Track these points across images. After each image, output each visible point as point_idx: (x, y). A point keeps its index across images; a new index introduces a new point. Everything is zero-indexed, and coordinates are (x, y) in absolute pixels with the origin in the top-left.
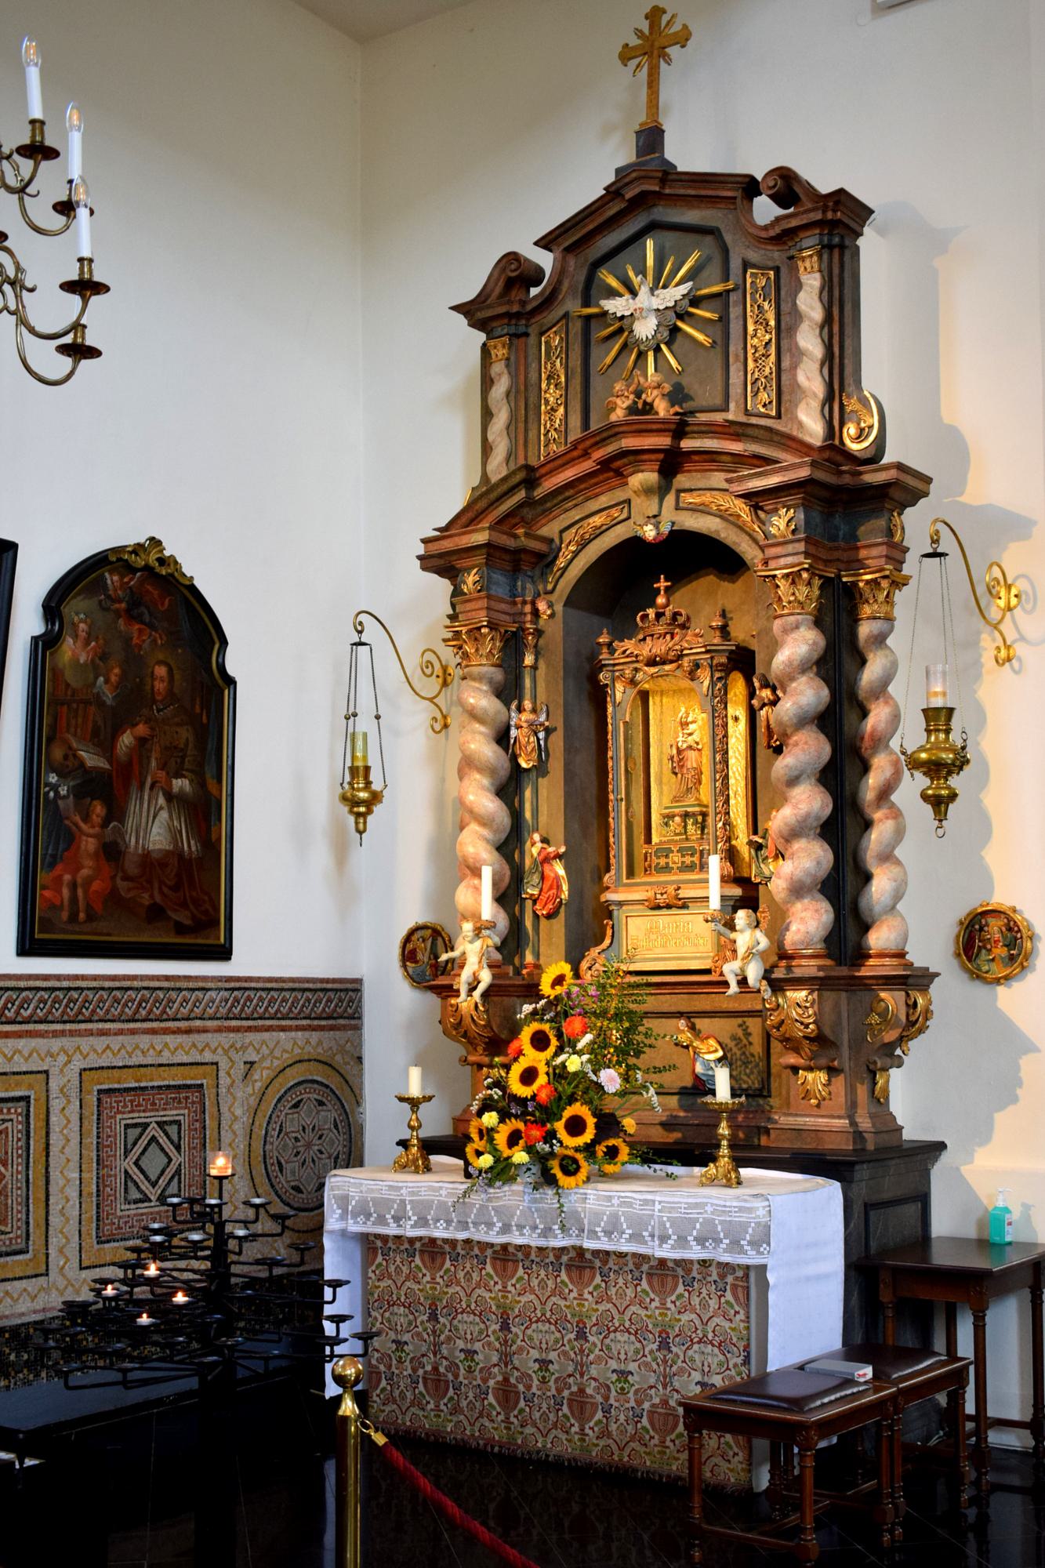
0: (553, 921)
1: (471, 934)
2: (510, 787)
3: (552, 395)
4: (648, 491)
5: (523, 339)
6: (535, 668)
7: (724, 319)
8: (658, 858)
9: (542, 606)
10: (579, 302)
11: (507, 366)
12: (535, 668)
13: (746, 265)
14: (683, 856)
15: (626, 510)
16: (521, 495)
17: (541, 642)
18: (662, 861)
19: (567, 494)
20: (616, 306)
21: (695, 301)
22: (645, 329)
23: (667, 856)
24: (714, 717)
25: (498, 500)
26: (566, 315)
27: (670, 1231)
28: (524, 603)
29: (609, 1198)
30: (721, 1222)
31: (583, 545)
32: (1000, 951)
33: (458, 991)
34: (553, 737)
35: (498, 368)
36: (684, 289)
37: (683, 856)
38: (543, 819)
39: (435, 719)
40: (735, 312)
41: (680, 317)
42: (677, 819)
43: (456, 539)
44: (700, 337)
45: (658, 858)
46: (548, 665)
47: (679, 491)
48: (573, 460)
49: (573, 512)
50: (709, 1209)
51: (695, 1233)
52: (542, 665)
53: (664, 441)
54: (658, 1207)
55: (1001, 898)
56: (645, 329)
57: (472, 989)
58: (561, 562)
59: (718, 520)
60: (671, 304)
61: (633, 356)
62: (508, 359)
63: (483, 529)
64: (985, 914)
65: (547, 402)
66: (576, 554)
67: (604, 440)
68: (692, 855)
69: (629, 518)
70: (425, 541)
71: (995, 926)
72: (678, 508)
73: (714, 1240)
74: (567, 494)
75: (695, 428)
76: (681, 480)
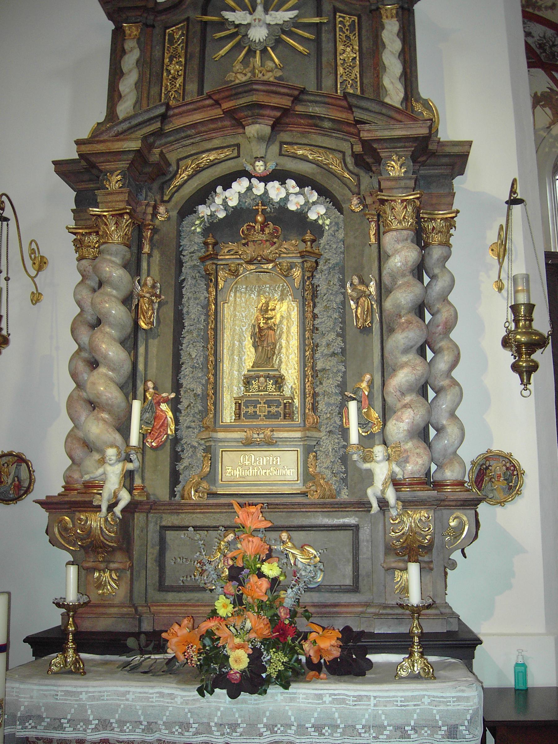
0: (160, 452)
1: (114, 458)
2: (131, 340)
3: (174, 68)
4: (260, 138)
5: (150, 29)
6: (150, 255)
7: (318, 41)
8: (247, 407)
9: (162, 209)
10: (199, 11)
11: (138, 43)
12: (150, 255)
13: (335, 10)
14: (269, 407)
15: (236, 151)
16: (157, 125)
17: (156, 237)
18: (251, 410)
19: (189, 132)
20: (238, 17)
21: (298, 25)
22: (258, 34)
23: (255, 407)
24: (304, 305)
25: (137, 125)
26: (188, 19)
27: (91, 718)
28: (148, 205)
29: (320, 697)
30: (91, 706)
31: (198, 171)
32: (501, 484)
33: (99, 507)
34: (164, 309)
35: (130, 44)
36: (292, 14)
37: (269, 407)
38: (152, 371)
39: (33, 293)
40: (325, 37)
41: (284, 32)
42: (262, 379)
43: (109, 144)
44: (300, 48)
45: (247, 407)
46: (162, 254)
47: (282, 143)
48: (203, 107)
49: (190, 148)
50: (426, 700)
51: (313, 720)
52: (157, 255)
53: (286, 102)
54: (373, 702)
55: (495, 448)
56: (258, 34)
57: (111, 507)
58: (177, 182)
59: (314, 166)
60: (281, 22)
61: (244, 52)
62: (139, 39)
63: (136, 139)
64: (487, 459)
65: (169, 72)
66: (190, 177)
67: (236, 94)
68: (277, 407)
69: (238, 156)
70: (79, 143)
71: (497, 468)
72: (281, 154)
73: (330, 726)
74: (189, 132)
75: (312, 98)
76: (285, 137)
